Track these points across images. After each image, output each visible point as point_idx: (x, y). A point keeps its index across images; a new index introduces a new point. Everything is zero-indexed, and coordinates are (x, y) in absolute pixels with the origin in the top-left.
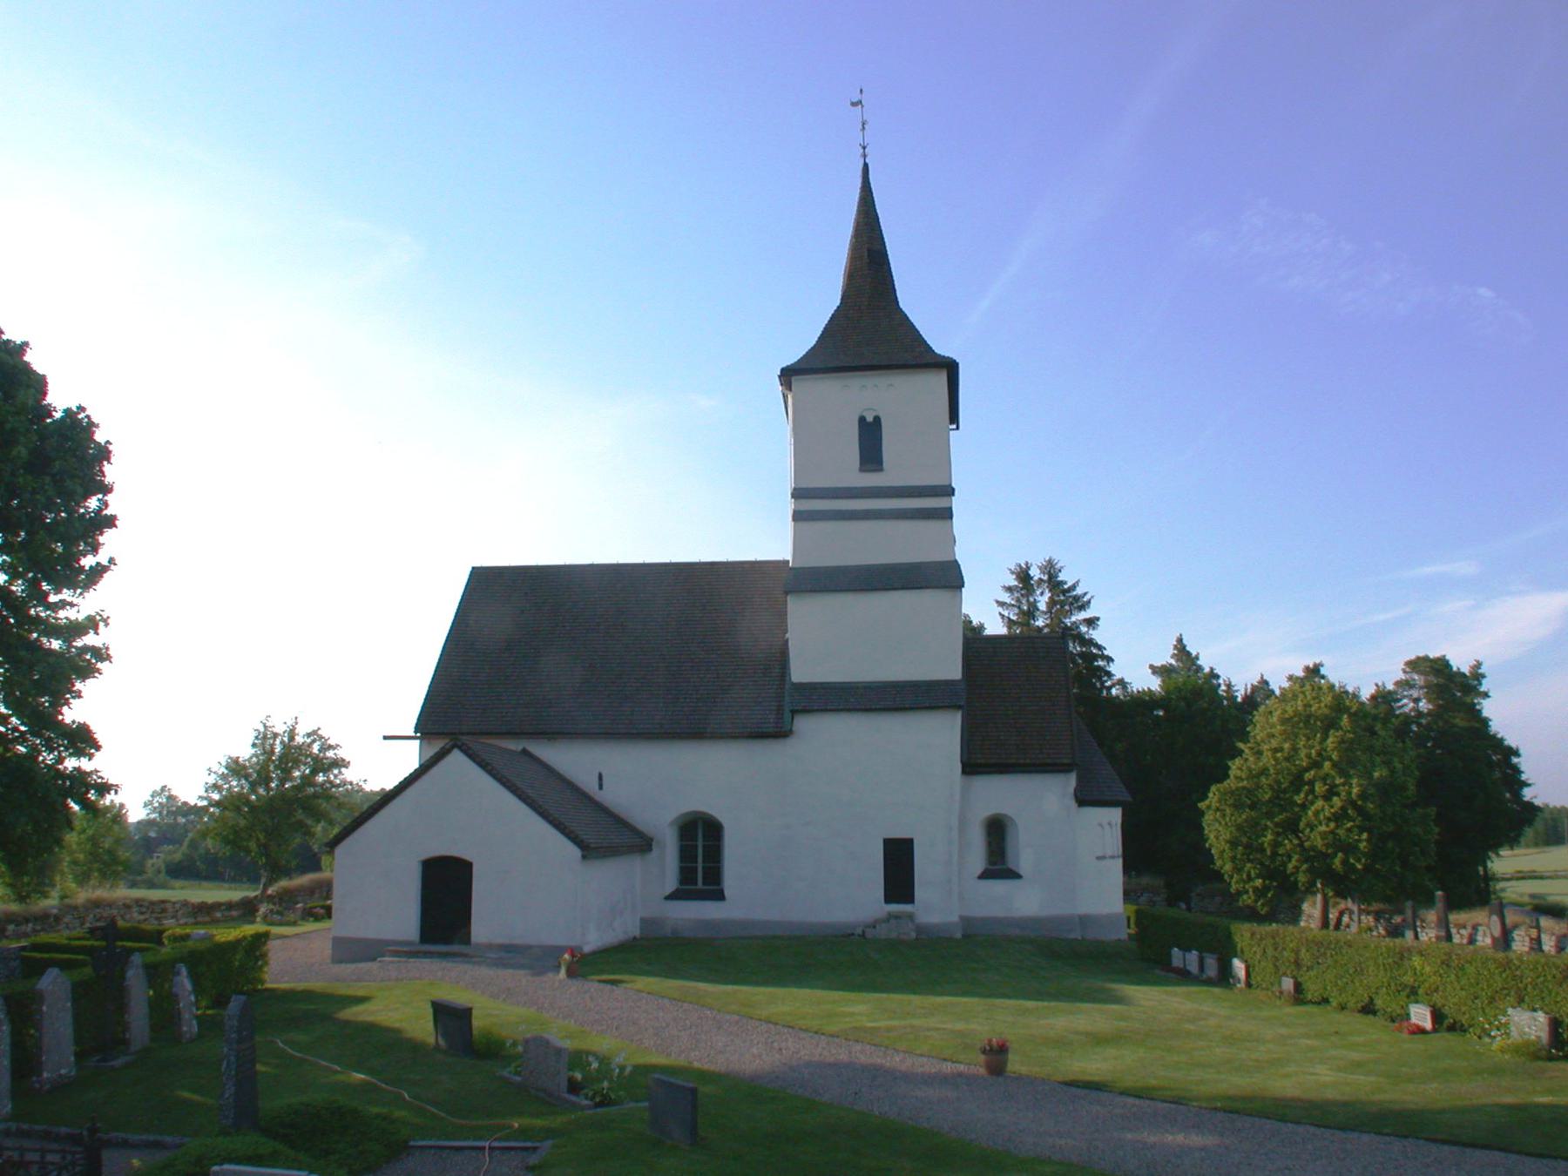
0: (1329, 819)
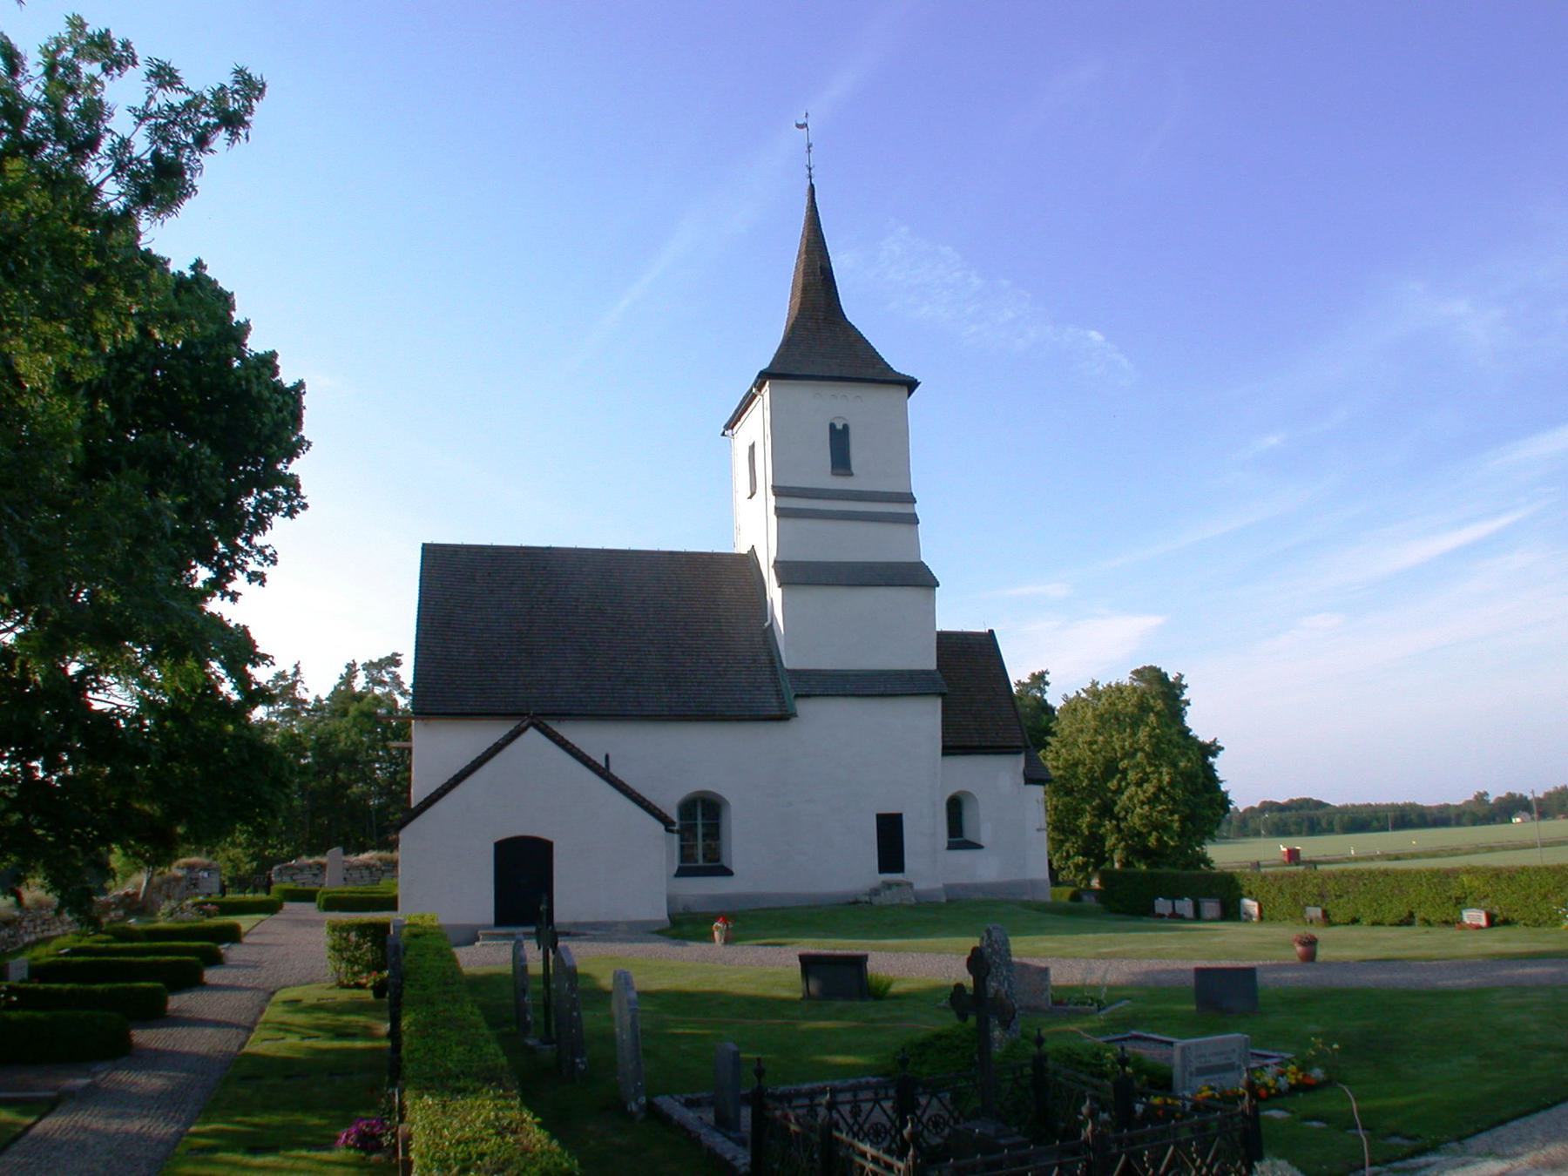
0: (1143, 803)
